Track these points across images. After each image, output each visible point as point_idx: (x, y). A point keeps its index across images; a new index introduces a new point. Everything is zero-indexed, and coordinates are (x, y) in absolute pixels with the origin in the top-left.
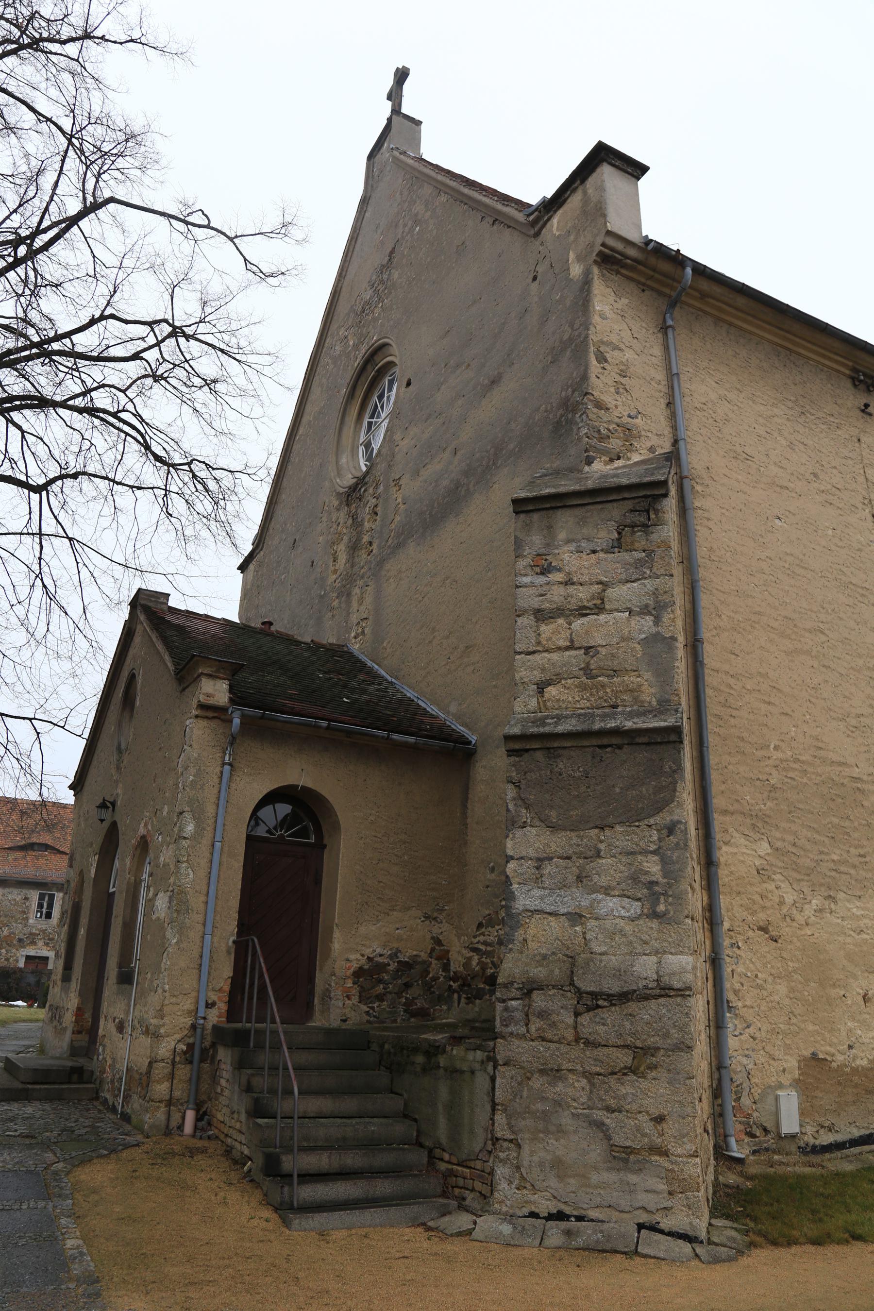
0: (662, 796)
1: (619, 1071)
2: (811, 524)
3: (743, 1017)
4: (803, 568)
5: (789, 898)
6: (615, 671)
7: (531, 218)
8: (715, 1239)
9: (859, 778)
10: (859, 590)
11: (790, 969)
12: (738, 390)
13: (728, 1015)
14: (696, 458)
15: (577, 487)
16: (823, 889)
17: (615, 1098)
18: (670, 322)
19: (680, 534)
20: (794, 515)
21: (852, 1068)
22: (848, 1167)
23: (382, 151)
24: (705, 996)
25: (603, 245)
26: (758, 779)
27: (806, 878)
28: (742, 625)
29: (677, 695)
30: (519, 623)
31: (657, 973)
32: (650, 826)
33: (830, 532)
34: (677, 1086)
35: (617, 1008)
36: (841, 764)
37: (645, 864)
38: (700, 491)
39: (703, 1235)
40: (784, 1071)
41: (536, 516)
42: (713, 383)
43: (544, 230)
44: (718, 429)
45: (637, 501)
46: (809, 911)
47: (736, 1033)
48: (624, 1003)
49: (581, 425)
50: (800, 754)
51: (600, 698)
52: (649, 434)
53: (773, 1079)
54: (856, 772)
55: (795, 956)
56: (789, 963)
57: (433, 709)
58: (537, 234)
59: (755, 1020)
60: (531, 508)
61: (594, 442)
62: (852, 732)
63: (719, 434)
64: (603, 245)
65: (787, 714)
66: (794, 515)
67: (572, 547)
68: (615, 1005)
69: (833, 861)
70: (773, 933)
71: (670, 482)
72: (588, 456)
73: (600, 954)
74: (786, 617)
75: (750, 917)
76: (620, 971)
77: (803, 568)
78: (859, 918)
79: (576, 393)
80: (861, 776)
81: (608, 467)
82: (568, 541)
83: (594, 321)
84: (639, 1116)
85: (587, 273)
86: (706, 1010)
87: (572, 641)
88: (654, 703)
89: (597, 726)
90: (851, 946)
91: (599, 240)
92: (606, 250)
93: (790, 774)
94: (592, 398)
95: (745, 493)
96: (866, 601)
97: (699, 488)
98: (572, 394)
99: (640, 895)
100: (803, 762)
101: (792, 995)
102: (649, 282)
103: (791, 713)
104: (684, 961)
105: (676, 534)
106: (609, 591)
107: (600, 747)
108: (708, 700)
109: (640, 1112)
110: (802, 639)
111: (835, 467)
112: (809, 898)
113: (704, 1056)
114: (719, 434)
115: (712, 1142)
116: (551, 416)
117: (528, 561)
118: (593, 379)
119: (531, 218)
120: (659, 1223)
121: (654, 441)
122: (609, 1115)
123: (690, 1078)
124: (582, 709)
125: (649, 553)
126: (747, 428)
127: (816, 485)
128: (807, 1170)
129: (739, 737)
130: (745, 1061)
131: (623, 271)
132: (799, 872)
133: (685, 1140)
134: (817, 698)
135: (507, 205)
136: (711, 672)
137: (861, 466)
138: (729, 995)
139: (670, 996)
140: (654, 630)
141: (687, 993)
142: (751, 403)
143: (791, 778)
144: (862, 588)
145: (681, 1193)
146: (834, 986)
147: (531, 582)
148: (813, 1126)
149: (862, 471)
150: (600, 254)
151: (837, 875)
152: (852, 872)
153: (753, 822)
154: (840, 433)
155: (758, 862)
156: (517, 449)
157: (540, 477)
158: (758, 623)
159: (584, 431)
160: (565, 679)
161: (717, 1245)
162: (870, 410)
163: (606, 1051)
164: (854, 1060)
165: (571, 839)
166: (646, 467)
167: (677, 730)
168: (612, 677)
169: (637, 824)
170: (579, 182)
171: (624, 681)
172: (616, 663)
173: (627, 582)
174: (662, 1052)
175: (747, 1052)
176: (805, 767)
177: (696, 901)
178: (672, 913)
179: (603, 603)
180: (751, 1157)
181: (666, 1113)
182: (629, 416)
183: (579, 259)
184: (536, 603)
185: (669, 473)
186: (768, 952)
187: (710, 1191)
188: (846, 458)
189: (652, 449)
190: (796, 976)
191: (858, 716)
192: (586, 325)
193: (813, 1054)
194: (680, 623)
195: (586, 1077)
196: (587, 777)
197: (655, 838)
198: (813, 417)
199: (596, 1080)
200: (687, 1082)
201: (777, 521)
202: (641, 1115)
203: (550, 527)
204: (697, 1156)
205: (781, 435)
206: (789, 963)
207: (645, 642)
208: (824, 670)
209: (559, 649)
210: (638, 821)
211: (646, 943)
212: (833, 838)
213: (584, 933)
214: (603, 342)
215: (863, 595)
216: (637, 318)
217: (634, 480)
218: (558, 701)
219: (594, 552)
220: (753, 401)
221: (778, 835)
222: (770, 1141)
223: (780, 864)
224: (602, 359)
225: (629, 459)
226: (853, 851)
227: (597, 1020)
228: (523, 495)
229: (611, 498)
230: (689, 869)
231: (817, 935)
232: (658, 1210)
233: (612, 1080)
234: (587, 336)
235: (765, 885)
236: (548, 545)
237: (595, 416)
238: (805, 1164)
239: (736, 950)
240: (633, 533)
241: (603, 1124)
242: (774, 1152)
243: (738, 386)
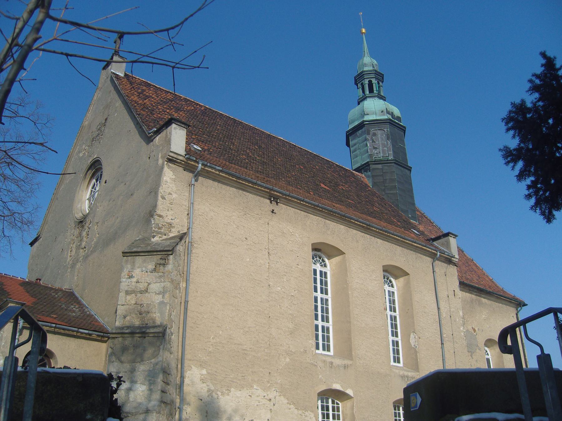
14: (195, 234)
16: (225, 387)
23: (108, 68)
30: (120, 294)
38: (196, 246)
41: (130, 258)
42: (208, 205)
45: (162, 255)
57: (100, 320)
63: (207, 225)
80: (247, 349)
82: (139, 267)
92: (170, 158)
102: (187, 167)
111: (255, 235)
140: (162, 300)
143: (217, 349)
144: (259, 280)
149: (267, 236)
151: (232, 383)
152: (238, 382)
153: (200, 363)
162: (274, 212)
183: (162, 157)
188: (261, 231)
191: (249, 328)
203: (134, 262)
210: (148, 361)
224: (163, 198)
236: (132, 269)
240: (160, 266)
243: (219, 205)
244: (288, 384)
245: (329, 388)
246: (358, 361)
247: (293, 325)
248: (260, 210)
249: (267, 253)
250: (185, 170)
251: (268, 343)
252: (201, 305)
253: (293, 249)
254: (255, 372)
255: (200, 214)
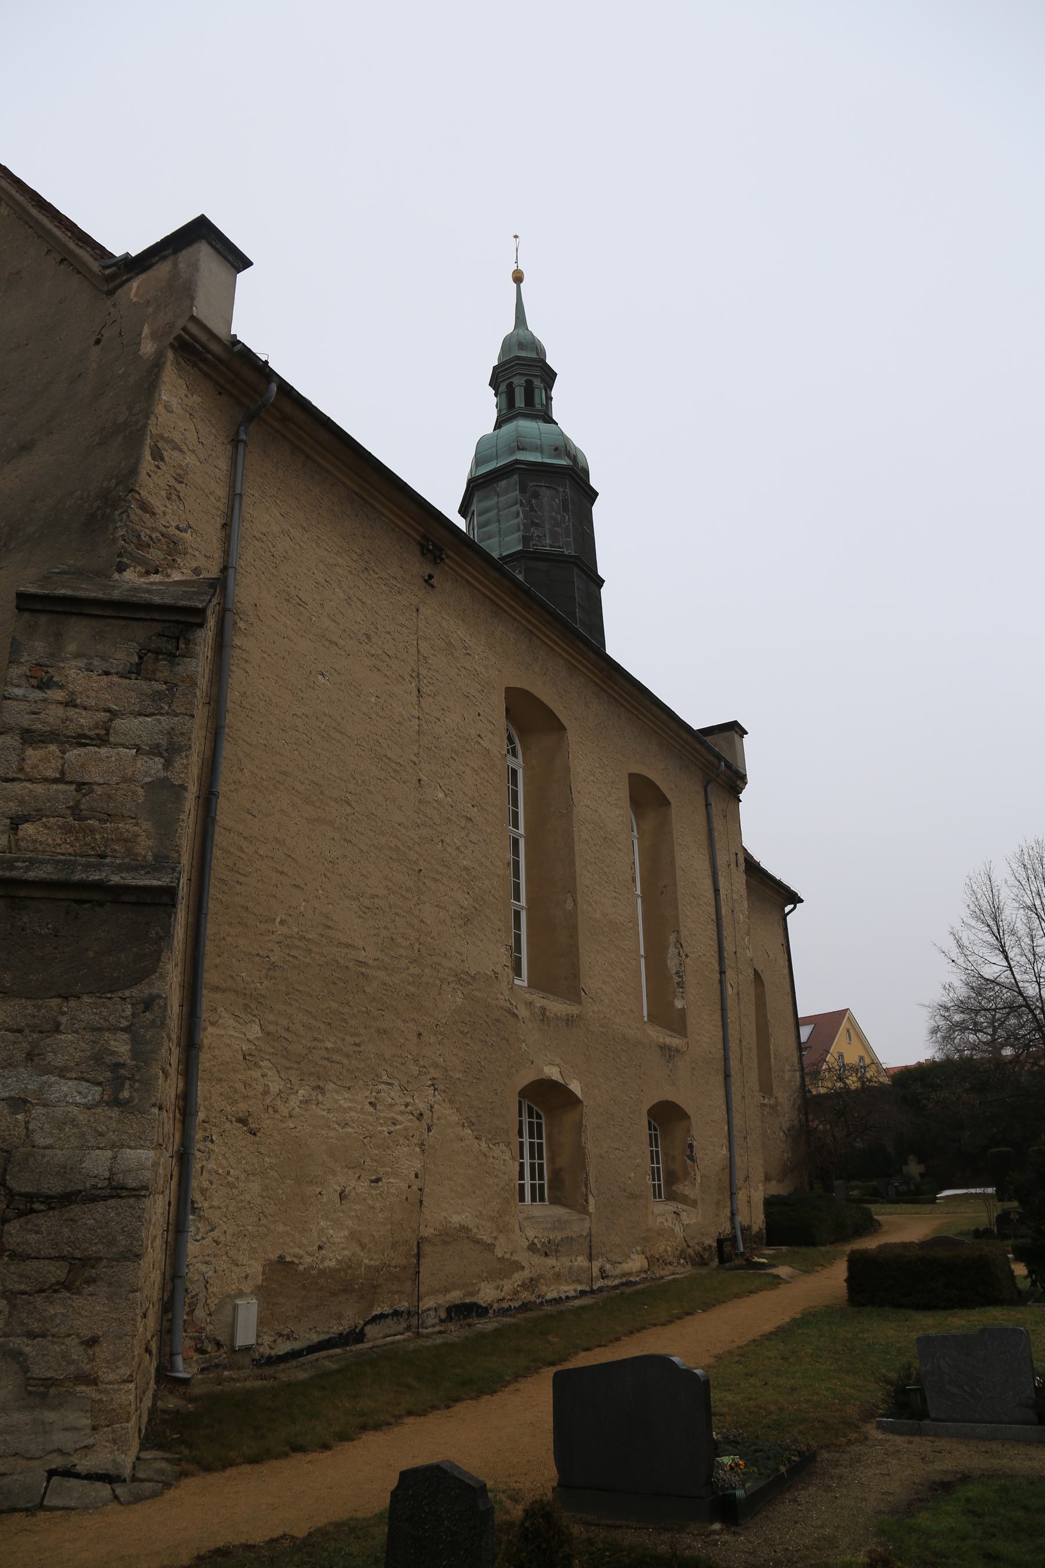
0: (143, 965)
1: (49, 1288)
2: (355, 687)
3: (207, 1219)
4: (340, 732)
5: (274, 1088)
6: (109, 815)
7: (107, 272)
8: (141, 1475)
9: (364, 963)
10: (393, 765)
11: (266, 1165)
12: (304, 528)
13: (191, 1217)
15: (100, 595)
17: (40, 1321)
18: (243, 436)
19: (212, 671)
20: (339, 674)
21: (319, 1270)
22: (302, 1376)
24: (167, 1197)
25: (184, 329)
26: (258, 955)
27: (296, 1066)
28: (265, 783)
29: (178, 852)
31: (110, 1170)
32: (124, 999)
33: (373, 699)
34: (118, 1301)
35: (56, 1213)
36: (348, 946)
37: (112, 1042)
38: (243, 628)
39: (127, 1472)
40: (247, 1277)
41: (43, 619)
42: (278, 515)
43: (120, 291)
44: (275, 565)
46: (294, 1102)
47: (198, 1237)
48: (66, 1206)
49: (119, 524)
50: (307, 932)
51: (86, 844)
52: (197, 553)
53: (234, 1287)
54: (362, 955)
55: (273, 1151)
56: (266, 1159)
58: (111, 293)
59: (221, 1222)
60: (38, 607)
61: (131, 548)
62: (364, 913)
63: (274, 571)
64: (184, 329)
65: (299, 887)
66: (339, 674)
67: (81, 663)
68: (53, 1208)
69: (327, 1049)
70: (252, 1126)
71: (209, 612)
72: (120, 562)
73: (44, 1148)
74: (312, 781)
75: (229, 1108)
76: (65, 1168)
77: (340, 732)
78: (345, 1110)
79: (120, 488)
81: (142, 580)
82: (77, 656)
83: (156, 411)
84: (67, 1341)
85: (160, 355)
86: (166, 1213)
87: (63, 773)
88: (150, 858)
89: (78, 876)
90: (334, 1141)
91: (181, 323)
92: (187, 337)
93: (293, 953)
94: (137, 496)
95: (291, 641)
96: (398, 778)
97: (242, 625)
98: (116, 487)
99: (101, 1079)
100: (308, 940)
101: (264, 1194)
103: (303, 886)
104: (144, 1156)
105: (207, 670)
106: (118, 722)
107: (76, 901)
108: (214, 861)
109: (69, 1335)
110: (326, 808)
111: (389, 633)
112: (296, 1088)
113: (157, 1265)
114: (274, 571)
115: (154, 1364)
116: (86, 506)
117: (24, 669)
118: (143, 475)
119: (107, 272)
120: (75, 1465)
121: (201, 562)
122: (30, 1342)
123: (134, 1291)
124: (63, 854)
125: (172, 686)
126: (306, 571)
127: (367, 647)
128: (259, 1383)
129: (243, 907)
130: (204, 1268)
131: (202, 365)
132: (289, 1060)
133: (119, 1364)
134: (333, 873)
135: (81, 247)
136: (223, 831)
137: (416, 637)
138: (196, 1195)
139: (122, 1197)
141: (143, 1193)
142: (314, 545)
143: (293, 956)
144: (396, 763)
145: (108, 1426)
146: (311, 1183)
147: (24, 696)
148: (271, 1336)
149: (415, 642)
150: (179, 338)
151: (329, 1064)
152: (345, 1061)
153: (245, 1001)
154: (400, 599)
155: (245, 1047)
156: (37, 535)
157: (59, 573)
158: (282, 784)
159: (121, 532)
160: (48, 817)
161: (142, 1480)
162: (432, 581)
163: (35, 1263)
164: (322, 1261)
165: (25, 1008)
166: (186, 589)
167: (171, 892)
168: (105, 822)
169: (109, 995)
170: (171, 250)
171: (118, 828)
172: (112, 805)
173: (140, 714)
174: (104, 1262)
175: (207, 1258)
176: (310, 946)
177: (169, 1088)
178: (137, 1100)
179: (107, 734)
180: (199, 1377)
181: (100, 1334)
182: (178, 528)
183: (154, 336)
184: (25, 721)
185: (210, 601)
186: (245, 1147)
187: (145, 1418)
188: (402, 625)
189: (196, 571)
190: (272, 1173)
191: (373, 896)
192: (147, 413)
193: (280, 1257)
194: (195, 771)
195: (7, 1298)
196: (56, 936)
197: (128, 1012)
198: (376, 576)
199: (18, 1301)
200: (131, 1296)
201: (320, 677)
202: (70, 1338)
204: (131, 1381)
205: (341, 587)
206: (266, 1159)
207: (150, 787)
208: (345, 844)
209: (46, 780)
210: (111, 992)
211: (101, 1134)
212: (329, 1024)
213: (27, 1122)
214: (162, 437)
215: (395, 771)
216: (207, 422)
217: (168, 601)
218: (35, 841)
219: (107, 673)
220: (317, 544)
221: (271, 1018)
222: (223, 1355)
223: (270, 1050)
224: (158, 455)
225: (168, 576)
226: (348, 1039)
227: (29, 1227)
228: (32, 589)
229: (137, 616)
230: (163, 1051)
231: (299, 1128)
232: (76, 1450)
233: (39, 1299)
234: (145, 426)
235: (249, 1072)
237: (137, 519)
238: (263, 1378)
239: (209, 1144)
240: (157, 660)
241: (21, 1353)
242: (225, 1368)
243: (304, 525)
244: (460, 1068)
245: (540, 1078)
246: (589, 1005)
247: (471, 900)
248: (400, 569)
249: (415, 692)
250: (220, 394)
251: (416, 948)
252: (251, 814)
253: (470, 691)
254: (385, 1031)
255: (255, 533)
